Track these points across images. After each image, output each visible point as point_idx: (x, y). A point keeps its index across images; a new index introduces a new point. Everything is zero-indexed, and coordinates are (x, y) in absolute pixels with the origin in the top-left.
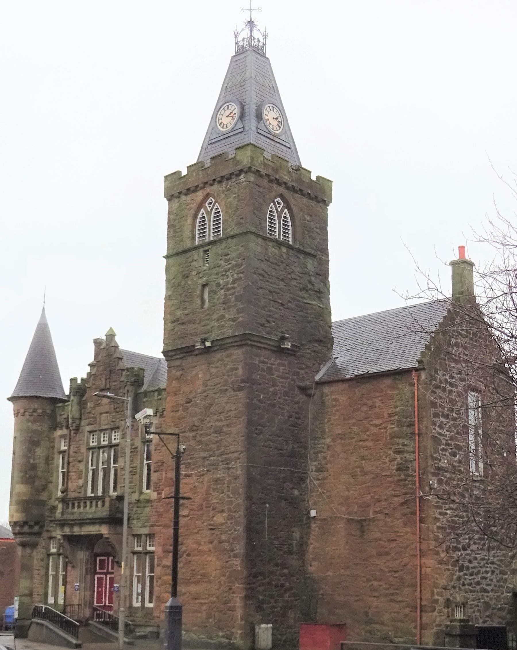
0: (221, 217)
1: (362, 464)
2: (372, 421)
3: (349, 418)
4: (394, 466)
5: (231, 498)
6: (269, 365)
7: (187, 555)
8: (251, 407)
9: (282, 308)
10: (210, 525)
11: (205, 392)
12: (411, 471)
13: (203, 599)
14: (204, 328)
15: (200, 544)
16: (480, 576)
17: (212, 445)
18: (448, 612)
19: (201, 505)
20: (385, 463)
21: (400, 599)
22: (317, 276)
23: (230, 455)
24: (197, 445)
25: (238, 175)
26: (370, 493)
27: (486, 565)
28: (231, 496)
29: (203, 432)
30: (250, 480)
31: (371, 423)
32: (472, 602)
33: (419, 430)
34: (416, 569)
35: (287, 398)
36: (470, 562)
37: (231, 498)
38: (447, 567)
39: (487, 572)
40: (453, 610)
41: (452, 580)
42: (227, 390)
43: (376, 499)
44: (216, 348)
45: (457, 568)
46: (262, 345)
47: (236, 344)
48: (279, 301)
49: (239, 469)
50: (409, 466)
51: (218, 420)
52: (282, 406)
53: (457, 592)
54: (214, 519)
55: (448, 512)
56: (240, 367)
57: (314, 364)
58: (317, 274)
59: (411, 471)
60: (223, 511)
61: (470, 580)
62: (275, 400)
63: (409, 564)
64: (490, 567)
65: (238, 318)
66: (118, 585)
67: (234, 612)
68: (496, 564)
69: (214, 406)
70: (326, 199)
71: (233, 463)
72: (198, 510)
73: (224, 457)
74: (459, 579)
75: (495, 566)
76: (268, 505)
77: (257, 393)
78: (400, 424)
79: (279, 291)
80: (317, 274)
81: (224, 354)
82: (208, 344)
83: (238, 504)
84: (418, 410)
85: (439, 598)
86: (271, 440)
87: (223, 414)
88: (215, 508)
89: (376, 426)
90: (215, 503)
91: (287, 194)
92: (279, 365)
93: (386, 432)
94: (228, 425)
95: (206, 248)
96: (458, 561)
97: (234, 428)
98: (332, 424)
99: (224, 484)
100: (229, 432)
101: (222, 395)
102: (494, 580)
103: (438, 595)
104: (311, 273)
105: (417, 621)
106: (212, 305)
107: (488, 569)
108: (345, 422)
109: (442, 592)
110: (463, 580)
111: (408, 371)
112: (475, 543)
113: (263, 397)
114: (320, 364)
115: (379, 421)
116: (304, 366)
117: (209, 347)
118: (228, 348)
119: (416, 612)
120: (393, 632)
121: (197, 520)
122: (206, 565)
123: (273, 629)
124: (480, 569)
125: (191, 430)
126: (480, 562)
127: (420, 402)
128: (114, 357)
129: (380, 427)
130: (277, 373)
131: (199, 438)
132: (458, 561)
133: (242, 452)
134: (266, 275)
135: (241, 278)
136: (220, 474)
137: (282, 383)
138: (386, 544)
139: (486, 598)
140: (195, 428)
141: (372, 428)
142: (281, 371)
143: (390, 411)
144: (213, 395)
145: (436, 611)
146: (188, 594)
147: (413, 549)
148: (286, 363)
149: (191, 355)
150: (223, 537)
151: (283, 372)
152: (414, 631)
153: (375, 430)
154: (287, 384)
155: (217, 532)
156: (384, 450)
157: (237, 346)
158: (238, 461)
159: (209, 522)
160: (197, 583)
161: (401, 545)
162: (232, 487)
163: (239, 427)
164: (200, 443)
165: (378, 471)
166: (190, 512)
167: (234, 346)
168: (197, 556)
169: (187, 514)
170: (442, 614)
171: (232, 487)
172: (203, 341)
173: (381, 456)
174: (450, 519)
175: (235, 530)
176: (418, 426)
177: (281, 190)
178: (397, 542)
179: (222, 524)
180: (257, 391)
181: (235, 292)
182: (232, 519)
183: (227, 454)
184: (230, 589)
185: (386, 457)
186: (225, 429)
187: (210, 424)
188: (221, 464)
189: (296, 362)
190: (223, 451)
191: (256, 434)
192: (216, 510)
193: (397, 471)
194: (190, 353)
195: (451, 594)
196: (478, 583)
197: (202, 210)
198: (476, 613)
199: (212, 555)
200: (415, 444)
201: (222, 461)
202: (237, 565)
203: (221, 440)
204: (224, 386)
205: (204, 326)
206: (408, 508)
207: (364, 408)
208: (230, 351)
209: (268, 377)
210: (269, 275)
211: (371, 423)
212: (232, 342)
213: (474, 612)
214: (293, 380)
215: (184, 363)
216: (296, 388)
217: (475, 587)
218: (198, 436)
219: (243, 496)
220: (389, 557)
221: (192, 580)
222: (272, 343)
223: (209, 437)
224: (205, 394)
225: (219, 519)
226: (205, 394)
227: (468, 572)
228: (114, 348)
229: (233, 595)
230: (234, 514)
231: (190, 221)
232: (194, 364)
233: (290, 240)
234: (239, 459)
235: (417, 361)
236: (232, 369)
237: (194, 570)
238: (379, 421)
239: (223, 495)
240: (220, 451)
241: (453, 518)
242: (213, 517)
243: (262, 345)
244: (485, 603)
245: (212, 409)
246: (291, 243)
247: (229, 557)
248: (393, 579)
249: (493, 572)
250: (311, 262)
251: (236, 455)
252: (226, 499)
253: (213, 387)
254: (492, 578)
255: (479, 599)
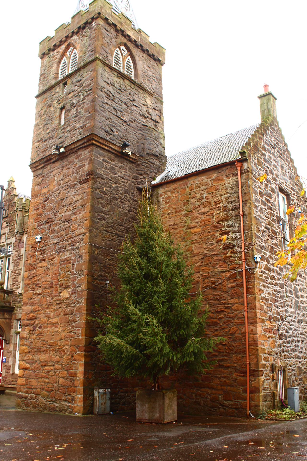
0: (77, 55)
1: (192, 247)
2: (200, 210)
3: (180, 211)
4: (220, 246)
5: (76, 274)
6: (112, 165)
7: (40, 328)
8: (95, 198)
9: (125, 124)
10: (58, 300)
11: (58, 190)
12: (236, 248)
13: (50, 366)
14: (60, 139)
15: (49, 317)
16: (294, 344)
17: (62, 232)
18: (273, 376)
19: (52, 284)
20: (212, 244)
21: (229, 364)
22: (154, 110)
23: (76, 238)
24: (50, 234)
25: (90, 23)
26: (199, 272)
27: (298, 335)
28: (75, 273)
29: (55, 222)
30: (92, 259)
31: (200, 212)
32: (290, 367)
33: (243, 211)
34: (245, 336)
35: (127, 195)
36: (287, 332)
37: (76, 274)
38: (271, 335)
39: (298, 341)
40: (276, 374)
41: (274, 347)
42: (75, 184)
43: (205, 276)
44: (68, 153)
45: (278, 336)
46: (106, 148)
47: (83, 146)
48: (122, 118)
49: (83, 248)
50: (235, 244)
51: (67, 211)
52: (123, 201)
53: (278, 358)
54: (62, 294)
55: (269, 285)
56: (86, 164)
57: (151, 172)
58: (154, 108)
59: (236, 248)
60: (68, 287)
61: (287, 347)
62: (117, 194)
63: (237, 332)
64: (301, 337)
65: (86, 125)
66: (5, 357)
67: (75, 378)
68: (304, 335)
69: (65, 200)
70: (161, 59)
71: (78, 244)
72: (49, 288)
73: (70, 240)
74: (280, 346)
75: (303, 336)
76: (108, 282)
77: (100, 185)
78: (225, 209)
79: (122, 110)
80: (154, 108)
81: (74, 156)
82: (62, 150)
83: (81, 280)
84: (242, 195)
85: (266, 363)
86: (112, 227)
87: (71, 205)
88: (62, 285)
89: (204, 214)
90: (61, 280)
91: (129, 44)
92: (121, 168)
93: (213, 217)
94: (75, 214)
95: (64, 82)
96: (278, 330)
97: (80, 215)
98: (166, 217)
99: (70, 263)
100: (75, 219)
101: (71, 190)
102: (304, 348)
103: (265, 360)
104: (149, 106)
105: (246, 385)
106: (66, 121)
107: (299, 339)
108: (177, 214)
109: (267, 357)
110: (282, 347)
111: (232, 164)
112: (289, 316)
113: (106, 190)
114: (156, 174)
115: (207, 209)
116: (143, 173)
117: (63, 153)
118: (77, 151)
119: (246, 376)
120: (222, 396)
121: (48, 296)
122: (53, 335)
123: (111, 393)
124: (294, 338)
125: (47, 223)
126: (294, 332)
127: (244, 188)
128: (12, 194)
129: (207, 214)
130: (119, 174)
131: (52, 228)
132: (278, 330)
133: (85, 234)
134: (111, 95)
135: (90, 94)
136: (67, 255)
137: (124, 182)
138: (215, 315)
139: (299, 364)
140: (50, 220)
141: (200, 216)
142: (123, 173)
143: (216, 200)
144: (64, 191)
145: (264, 375)
146: (38, 362)
147: (240, 318)
148: (127, 168)
149: (50, 163)
150: (69, 310)
151: (124, 175)
152: (242, 394)
153: (203, 217)
154: (128, 184)
155: (63, 306)
156: (211, 233)
157: (85, 147)
158: (82, 242)
159: (57, 298)
160: (45, 352)
161: (229, 315)
162: (76, 264)
163: (85, 213)
164: (53, 231)
165: (206, 252)
166: (43, 290)
167: (82, 148)
168: (47, 328)
169: (40, 292)
170: (268, 378)
171: (76, 264)
172: (58, 149)
173: (209, 239)
174: (271, 292)
175: (78, 303)
176: (243, 208)
177: (125, 41)
178: (225, 313)
179: (67, 298)
180: (100, 184)
181: (84, 107)
182: (75, 293)
183: (73, 238)
184: (72, 356)
185: (213, 239)
186: (73, 217)
187: (61, 215)
188: (68, 246)
189: (136, 169)
190: (71, 236)
191: (99, 219)
192: (63, 287)
193: (223, 250)
194: (49, 162)
195: (274, 360)
196: (293, 350)
197: (65, 58)
198: (293, 377)
199: (59, 326)
200: (240, 224)
201: (69, 244)
202: (78, 335)
203: (69, 227)
204: (73, 182)
205: (60, 138)
206: (235, 281)
207: (193, 200)
208: (80, 153)
209: (111, 174)
210: (113, 95)
211: (200, 212)
212: (81, 145)
213: (291, 376)
214: (133, 182)
215: (45, 171)
216: (136, 190)
217: (291, 354)
218: (52, 227)
219: (85, 271)
220: (217, 327)
221: (43, 349)
222: (116, 148)
223: (60, 225)
224: (58, 192)
225: (65, 294)
226: (58, 192)
227: (286, 340)
228: (12, 189)
229: (75, 362)
230: (77, 289)
231: (55, 66)
232: (52, 170)
233: (133, 76)
234: (82, 240)
235: (240, 153)
236: (80, 167)
237: (44, 340)
238: (207, 209)
239: (69, 272)
240: (68, 235)
241: (274, 292)
242: (60, 293)
243: (106, 148)
244: (299, 367)
245: (63, 203)
246: (133, 78)
247: (72, 328)
248: (222, 346)
249: (302, 341)
250: (149, 98)
251: (80, 237)
252: (71, 276)
253: (64, 185)
254: (302, 346)
255: (294, 364)
